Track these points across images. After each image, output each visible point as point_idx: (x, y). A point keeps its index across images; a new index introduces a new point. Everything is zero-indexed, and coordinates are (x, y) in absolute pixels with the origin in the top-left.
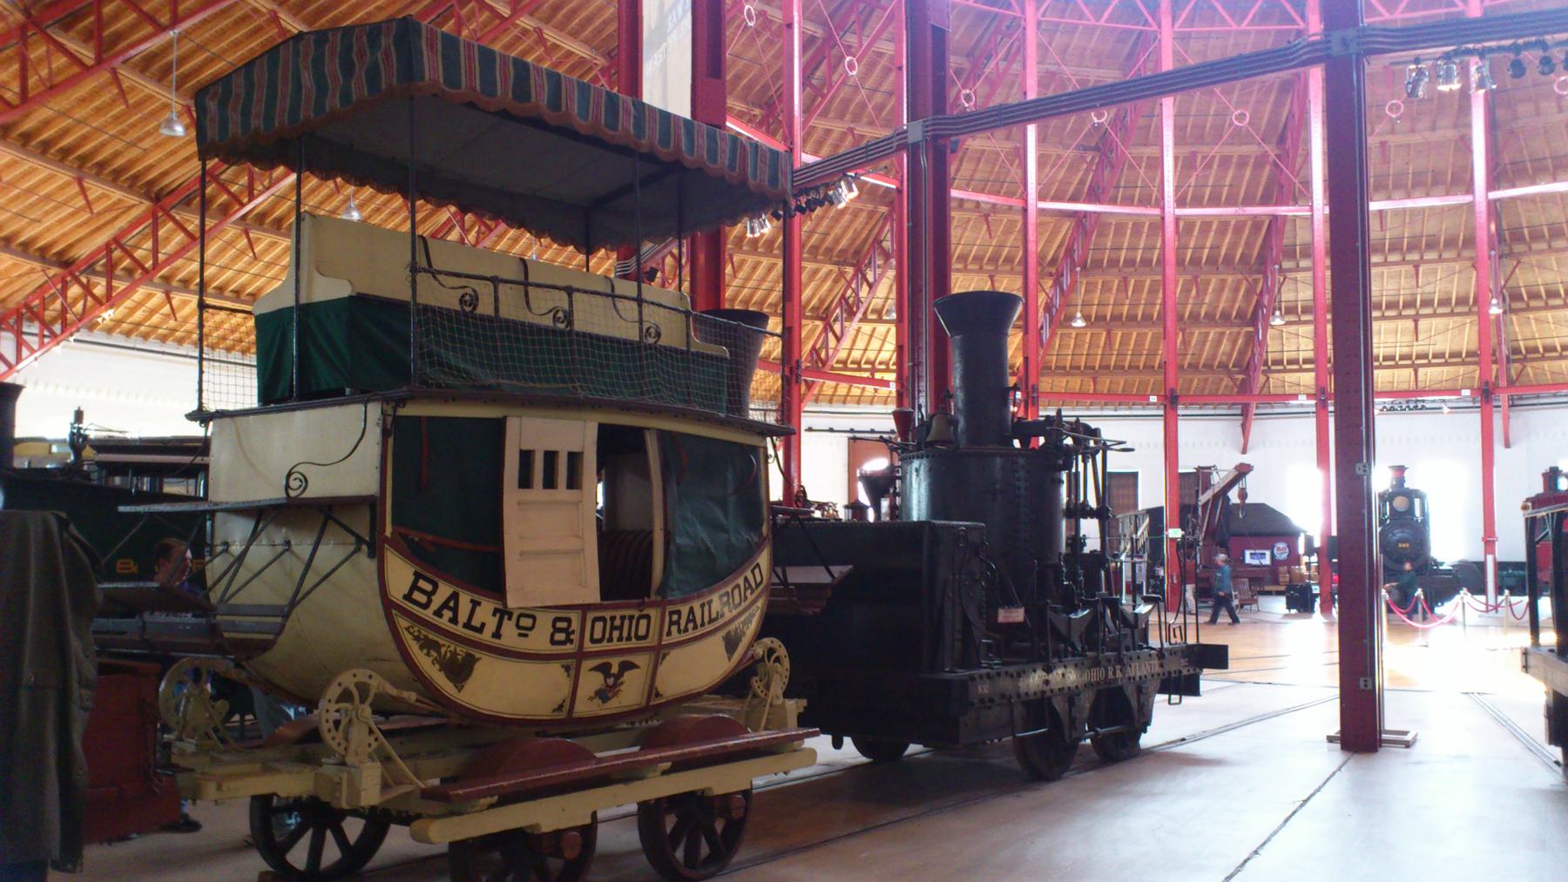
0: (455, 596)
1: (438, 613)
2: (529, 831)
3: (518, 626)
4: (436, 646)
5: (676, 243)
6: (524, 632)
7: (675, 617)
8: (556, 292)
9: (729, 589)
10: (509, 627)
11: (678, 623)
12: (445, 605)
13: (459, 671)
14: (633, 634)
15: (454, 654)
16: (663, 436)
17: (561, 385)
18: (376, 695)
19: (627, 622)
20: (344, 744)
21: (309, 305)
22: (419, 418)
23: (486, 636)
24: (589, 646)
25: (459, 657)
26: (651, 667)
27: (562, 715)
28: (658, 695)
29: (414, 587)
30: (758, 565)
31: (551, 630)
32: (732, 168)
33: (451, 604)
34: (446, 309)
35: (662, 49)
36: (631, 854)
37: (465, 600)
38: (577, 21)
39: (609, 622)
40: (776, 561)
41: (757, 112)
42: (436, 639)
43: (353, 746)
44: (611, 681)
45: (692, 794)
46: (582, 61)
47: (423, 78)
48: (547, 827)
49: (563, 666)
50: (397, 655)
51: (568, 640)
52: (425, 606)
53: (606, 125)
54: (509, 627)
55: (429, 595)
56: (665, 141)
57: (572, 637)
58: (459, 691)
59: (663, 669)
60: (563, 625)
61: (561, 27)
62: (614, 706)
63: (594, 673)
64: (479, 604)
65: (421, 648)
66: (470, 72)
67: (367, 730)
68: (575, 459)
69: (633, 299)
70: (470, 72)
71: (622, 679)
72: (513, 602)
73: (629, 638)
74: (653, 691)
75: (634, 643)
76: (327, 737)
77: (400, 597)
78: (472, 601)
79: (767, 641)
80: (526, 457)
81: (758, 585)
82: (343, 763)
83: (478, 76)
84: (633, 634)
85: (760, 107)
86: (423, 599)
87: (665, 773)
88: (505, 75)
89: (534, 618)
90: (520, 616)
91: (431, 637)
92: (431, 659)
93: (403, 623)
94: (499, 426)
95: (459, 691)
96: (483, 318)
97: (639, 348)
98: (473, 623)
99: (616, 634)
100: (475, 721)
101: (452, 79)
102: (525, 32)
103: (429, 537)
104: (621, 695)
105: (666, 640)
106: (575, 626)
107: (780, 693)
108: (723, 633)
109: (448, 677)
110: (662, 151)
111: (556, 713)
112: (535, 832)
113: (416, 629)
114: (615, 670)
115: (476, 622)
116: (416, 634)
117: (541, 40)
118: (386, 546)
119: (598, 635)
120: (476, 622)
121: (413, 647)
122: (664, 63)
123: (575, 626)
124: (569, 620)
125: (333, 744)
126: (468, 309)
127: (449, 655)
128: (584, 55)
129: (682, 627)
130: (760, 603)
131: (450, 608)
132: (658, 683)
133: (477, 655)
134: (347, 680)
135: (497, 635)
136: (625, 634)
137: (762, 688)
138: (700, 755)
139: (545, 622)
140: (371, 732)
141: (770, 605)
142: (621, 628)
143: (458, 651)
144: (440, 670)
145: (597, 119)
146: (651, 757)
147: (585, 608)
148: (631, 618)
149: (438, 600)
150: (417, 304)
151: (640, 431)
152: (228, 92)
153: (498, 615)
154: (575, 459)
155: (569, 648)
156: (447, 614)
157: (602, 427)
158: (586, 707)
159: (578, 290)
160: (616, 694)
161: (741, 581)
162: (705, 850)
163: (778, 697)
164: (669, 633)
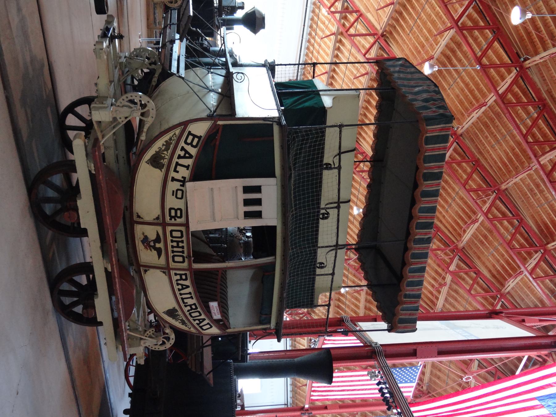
0: (191, 157)
1: (183, 149)
2: (78, 196)
3: (177, 190)
4: (167, 149)
5: (366, 284)
6: (175, 193)
7: (184, 277)
8: (335, 238)
9: (199, 309)
10: (177, 185)
11: (181, 279)
12: (186, 152)
13: (155, 162)
14: (175, 254)
15: (164, 158)
16: (273, 265)
17: (293, 196)
18: (144, 120)
19: (180, 250)
20: (121, 105)
21: (319, 95)
22: (273, 136)
23: (172, 174)
24: (169, 229)
25: (162, 161)
26: (160, 266)
27: (135, 218)
28: (146, 271)
29: (194, 136)
30: (211, 327)
31: (176, 208)
32: (406, 296)
33: (187, 155)
34: (325, 139)
35: (448, 328)
36: (68, 259)
37: (189, 162)
38: (452, 301)
39: (180, 240)
40: (214, 338)
41: (425, 388)
42: (171, 148)
43: (119, 109)
44: (152, 244)
45: (96, 290)
46: (435, 305)
47: (427, 125)
48: (79, 203)
49: (159, 216)
50: (163, 129)
51: (171, 217)
52: (186, 142)
53: (418, 223)
54: (177, 185)
55: (191, 144)
56: (415, 256)
57: (173, 219)
58: (146, 162)
59: (158, 272)
60: (179, 215)
61: (448, 293)
62: (140, 246)
63: (156, 233)
64: (188, 169)
65: (166, 141)
66: (433, 150)
67: (127, 116)
68: (258, 215)
69: (337, 242)
70: (433, 150)
71: (153, 250)
72: (189, 185)
73: (173, 252)
74: (148, 267)
75: (171, 255)
76: (124, 97)
77: (190, 130)
78: (189, 165)
79: (173, 336)
80: (258, 189)
81: (201, 327)
82: (112, 105)
83: (422, 251)
84: (175, 254)
85: (427, 390)
86: (189, 141)
87: (106, 269)
88: (432, 186)
89: (181, 198)
90: (182, 190)
91: (172, 146)
92: (161, 147)
93: (177, 131)
94: (273, 175)
95: (146, 162)
96: (315, 271)
97: (314, 246)
98: (178, 167)
99: (175, 244)
100: (132, 170)
101: (429, 140)
102: (444, 278)
103: (218, 143)
104: (145, 250)
105: (172, 272)
106: (179, 221)
107: (147, 345)
108: (177, 308)
109: (153, 155)
110: (407, 269)
111: (136, 215)
112: (77, 198)
113: (175, 138)
114: (158, 245)
115: (179, 168)
116: (173, 138)
117: (441, 285)
118: (213, 122)
119: (175, 234)
120: (179, 168)
121: (166, 137)
122: (441, 329)
123: (179, 221)
124: (181, 217)
125: (121, 100)
126: (321, 216)
127: (163, 155)
128: (438, 305)
129: (179, 282)
130: (192, 330)
131: (185, 154)
132: (152, 271)
133: (163, 170)
134: (151, 105)
135: (173, 179)
136: (175, 249)
137: (149, 334)
138: (114, 288)
139: (179, 204)
140: (126, 118)
141: (192, 335)
142: (178, 246)
143: (165, 160)
144: (156, 152)
145: (420, 218)
146: (114, 259)
147: (187, 225)
148: (183, 252)
149: (189, 148)
150: (325, 128)
151: (274, 254)
152: (407, 67)
153: (183, 179)
154: (258, 215)
155: (168, 218)
156: (182, 154)
157: (274, 228)
158: (139, 230)
159: (339, 211)
160: (146, 248)
161: (203, 316)
162: (67, 301)
163: (145, 343)
164: (176, 274)
